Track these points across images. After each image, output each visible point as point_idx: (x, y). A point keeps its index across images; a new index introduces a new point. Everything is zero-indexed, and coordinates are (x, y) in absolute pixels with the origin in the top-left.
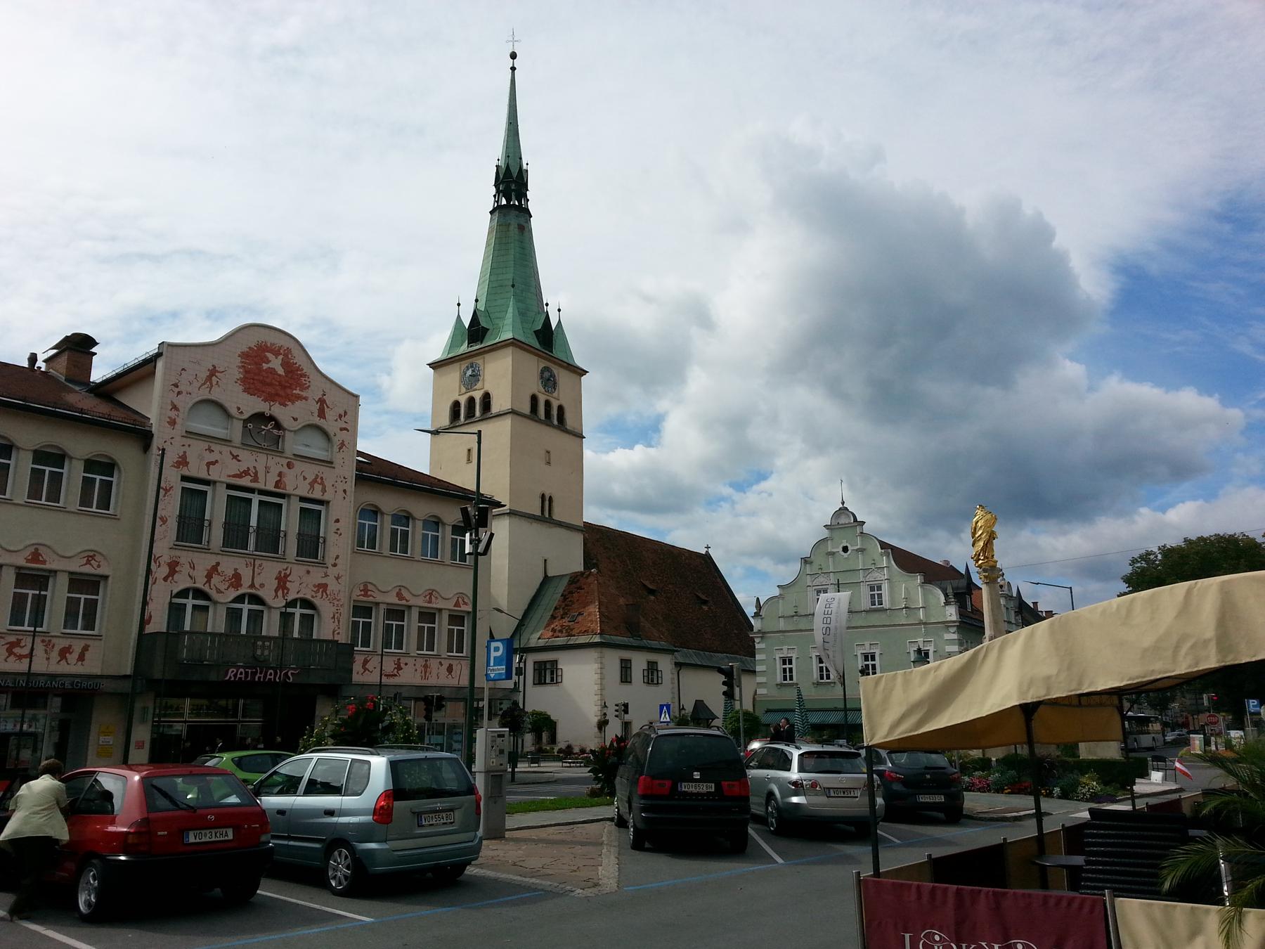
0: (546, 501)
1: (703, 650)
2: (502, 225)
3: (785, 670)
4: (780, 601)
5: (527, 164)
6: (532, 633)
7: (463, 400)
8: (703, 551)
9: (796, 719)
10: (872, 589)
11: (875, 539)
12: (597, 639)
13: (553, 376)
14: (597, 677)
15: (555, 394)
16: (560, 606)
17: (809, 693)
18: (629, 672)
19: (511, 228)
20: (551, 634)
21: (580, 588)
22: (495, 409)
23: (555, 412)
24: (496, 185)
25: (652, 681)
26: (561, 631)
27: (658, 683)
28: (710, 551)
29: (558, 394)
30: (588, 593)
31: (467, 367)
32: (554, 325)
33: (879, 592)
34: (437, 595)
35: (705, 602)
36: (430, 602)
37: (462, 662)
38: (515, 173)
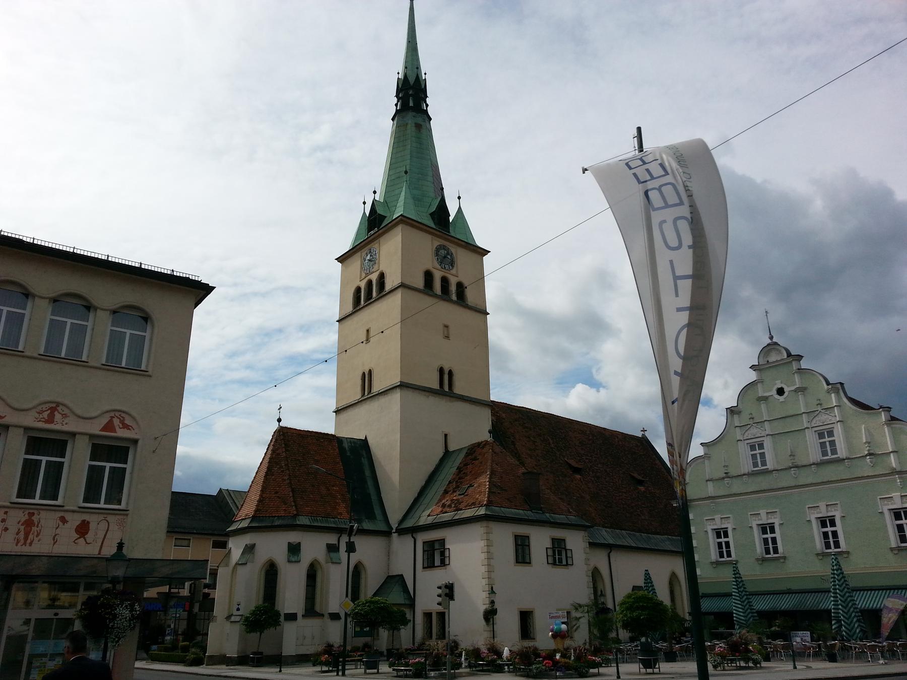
0: (446, 376)
1: (640, 531)
2: (401, 126)
3: (720, 544)
4: (706, 462)
5: (425, 74)
6: (423, 511)
7: (363, 285)
8: (640, 435)
9: (736, 607)
10: (821, 435)
11: (818, 375)
12: (482, 511)
13: (449, 253)
14: (483, 556)
15: (454, 271)
16: (454, 479)
17: (750, 571)
18: (527, 552)
19: (409, 126)
20: (440, 509)
21: (475, 459)
22: (388, 287)
23: (453, 288)
24: (397, 96)
25: (560, 561)
26: (450, 506)
27: (567, 564)
28: (647, 434)
29: (457, 271)
30: (481, 463)
31: (367, 253)
32: (453, 212)
33: (831, 439)
34: (66, 411)
35: (640, 482)
36: (50, 420)
37: (111, 519)
38: (412, 80)
